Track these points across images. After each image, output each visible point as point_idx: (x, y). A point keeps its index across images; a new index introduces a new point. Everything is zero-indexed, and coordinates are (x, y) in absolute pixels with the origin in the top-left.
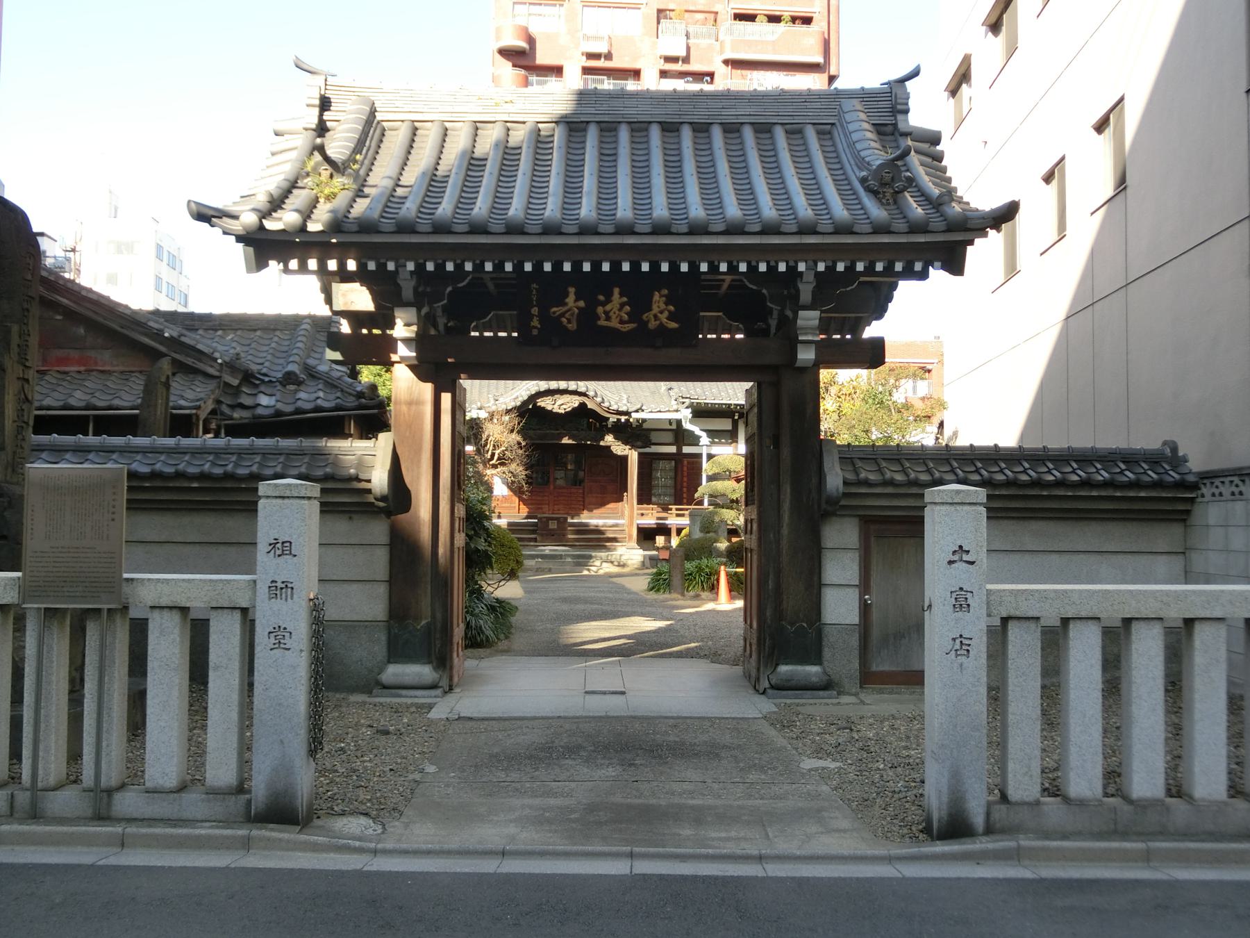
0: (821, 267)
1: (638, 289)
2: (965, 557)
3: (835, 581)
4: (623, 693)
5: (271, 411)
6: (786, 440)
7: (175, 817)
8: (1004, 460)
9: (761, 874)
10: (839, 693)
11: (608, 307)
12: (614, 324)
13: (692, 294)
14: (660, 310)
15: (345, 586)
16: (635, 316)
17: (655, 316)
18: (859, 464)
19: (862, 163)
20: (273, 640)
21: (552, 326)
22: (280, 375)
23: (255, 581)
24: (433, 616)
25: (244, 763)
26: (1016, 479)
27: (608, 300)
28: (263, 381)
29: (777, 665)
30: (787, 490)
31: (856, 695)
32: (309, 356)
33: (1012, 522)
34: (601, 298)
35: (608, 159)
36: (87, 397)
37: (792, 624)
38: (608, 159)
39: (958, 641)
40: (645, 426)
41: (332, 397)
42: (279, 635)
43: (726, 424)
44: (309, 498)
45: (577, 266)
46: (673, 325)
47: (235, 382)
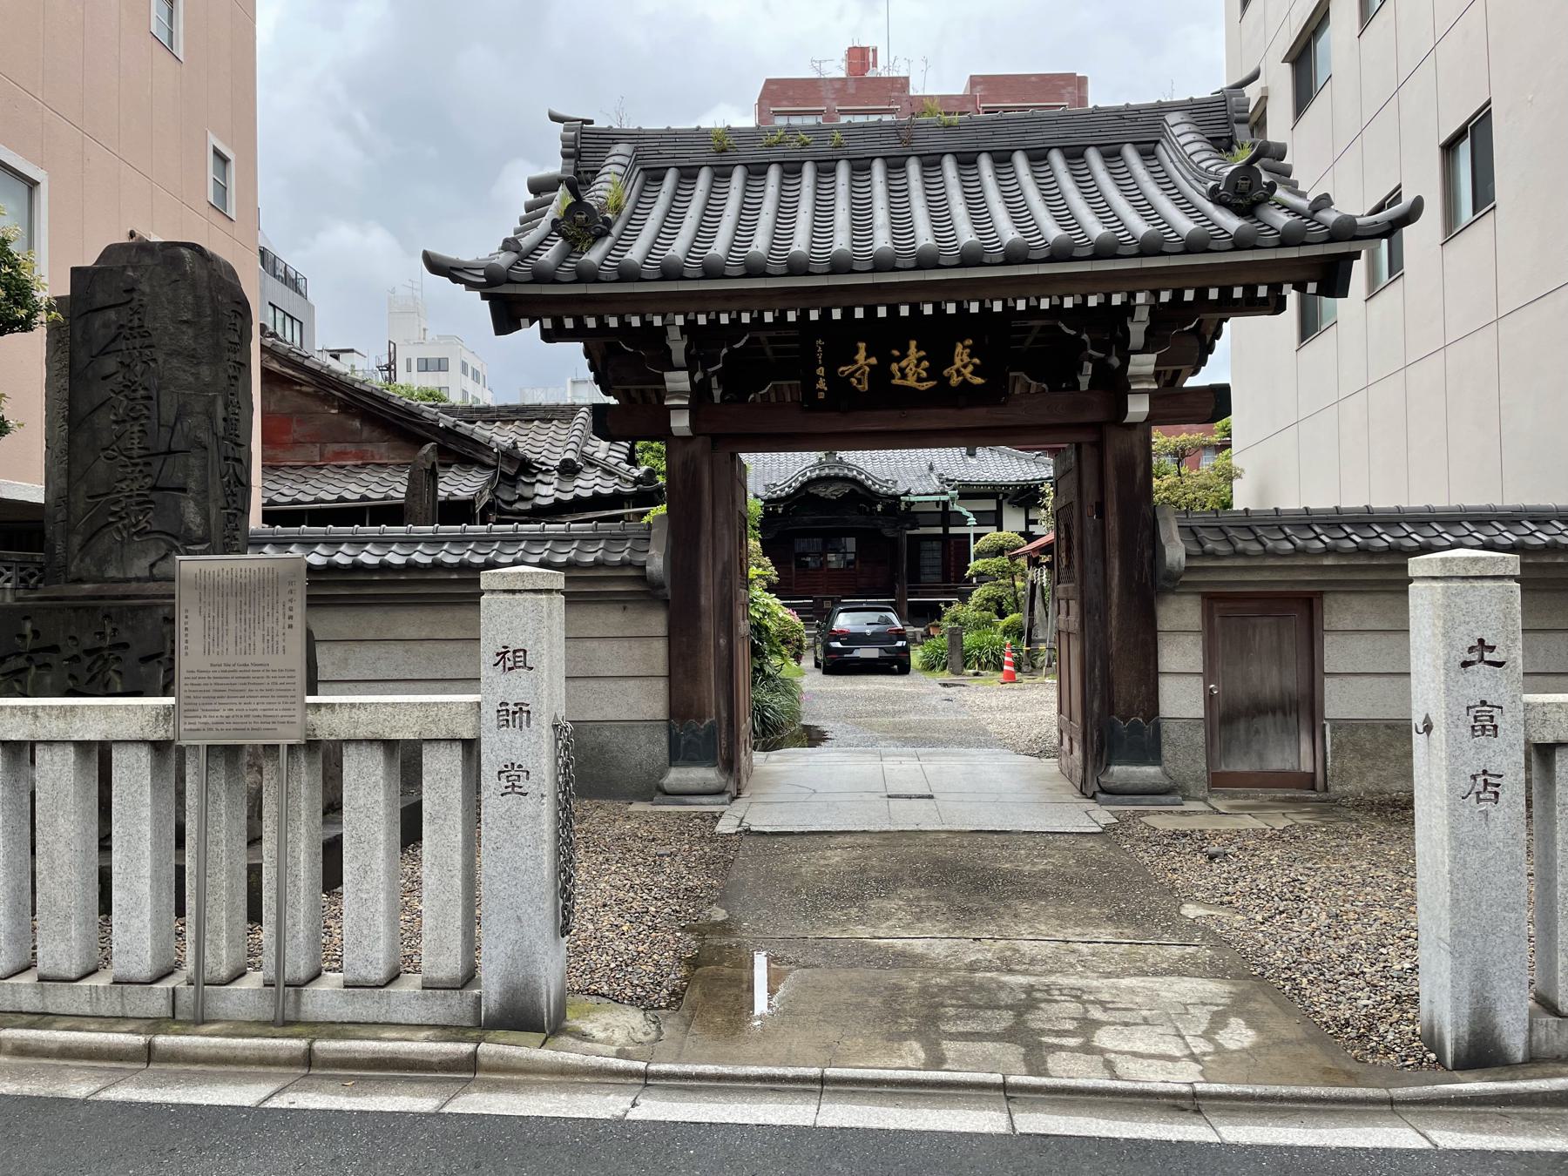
0: (1165, 297)
1: (938, 337)
2: (1488, 656)
3: (1174, 668)
4: (931, 797)
5: (550, 501)
6: (1112, 508)
7: (382, 1019)
8: (1378, 524)
9: (1213, 1138)
10: (1185, 798)
11: (904, 364)
12: (911, 382)
13: (1000, 338)
14: (963, 365)
15: (622, 683)
16: (933, 373)
17: (958, 371)
18: (1203, 533)
19: (1200, 175)
20: (504, 783)
21: (840, 386)
22: (557, 463)
23: (479, 704)
24: (718, 713)
25: (471, 945)
26: (1524, 543)
27: (904, 355)
28: (540, 470)
29: (1108, 765)
30: (1115, 564)
31: (1204, 800)
32: (586, 444)
33: (1388, 596)
34: (896, 353)
35: (898, 196)
36: (363, 490)
37: (1125, 719)
38: (898, 196)
39: (1480, 780)
40: (913, 509)
41: (610, 484)
42: (513, 775)
43: (991, 505)
44: (549, 591)
45: (870, 311)
46: (978, 381)
47: (512, 472)
